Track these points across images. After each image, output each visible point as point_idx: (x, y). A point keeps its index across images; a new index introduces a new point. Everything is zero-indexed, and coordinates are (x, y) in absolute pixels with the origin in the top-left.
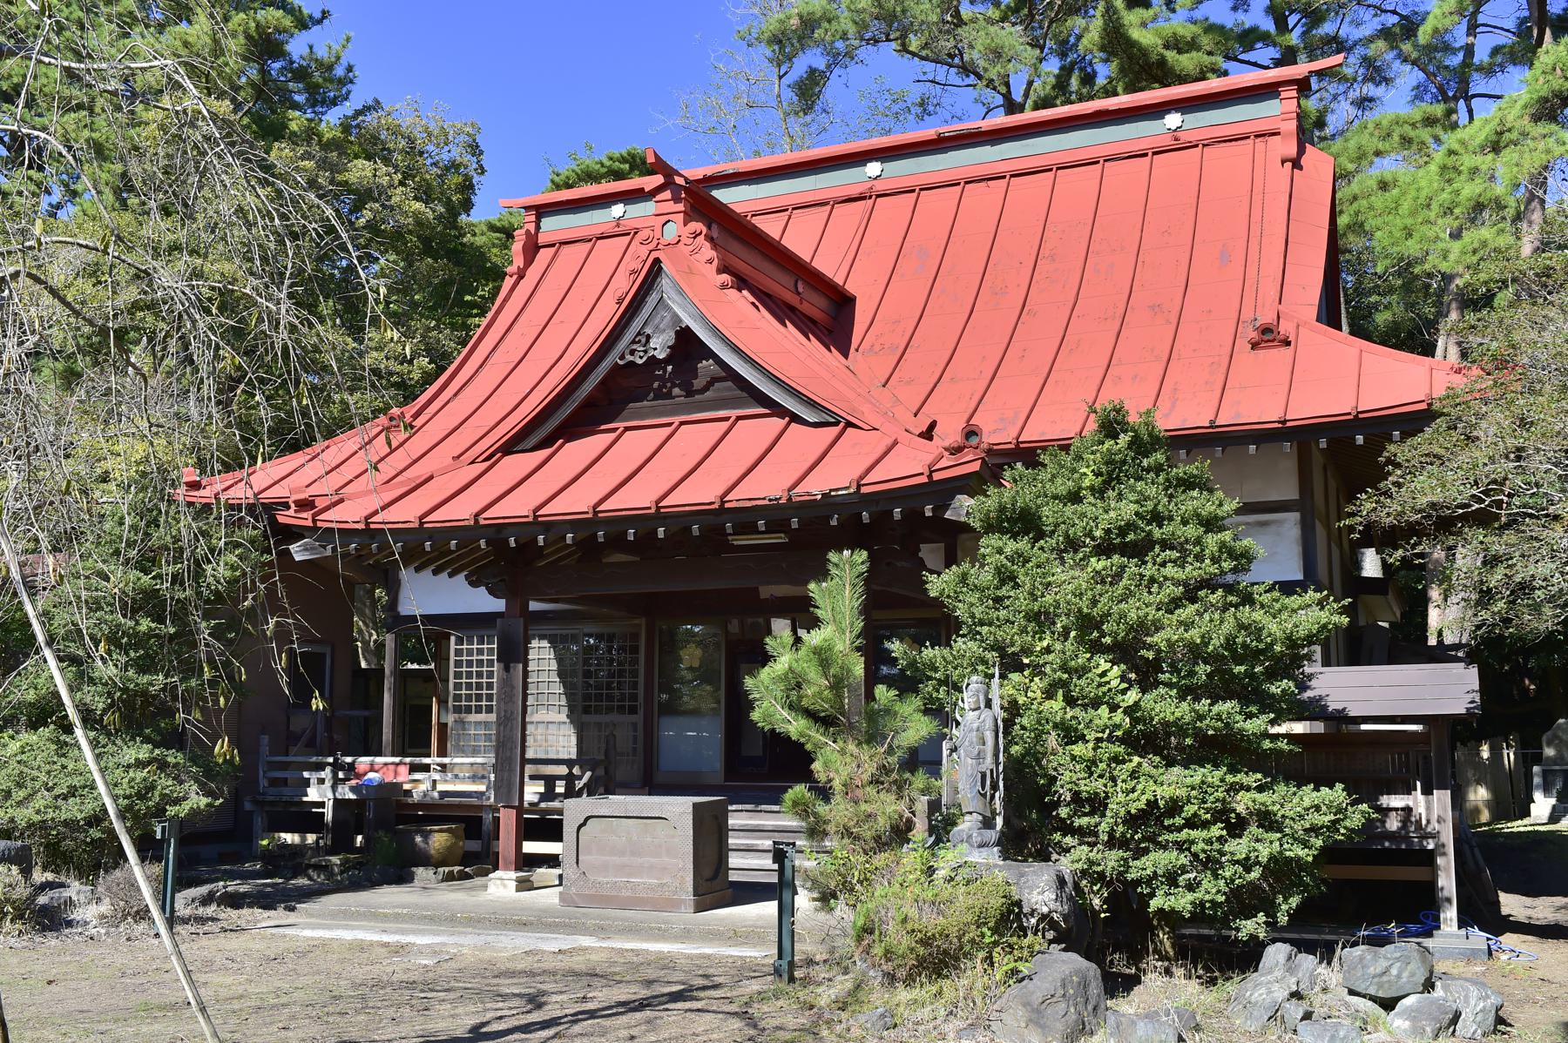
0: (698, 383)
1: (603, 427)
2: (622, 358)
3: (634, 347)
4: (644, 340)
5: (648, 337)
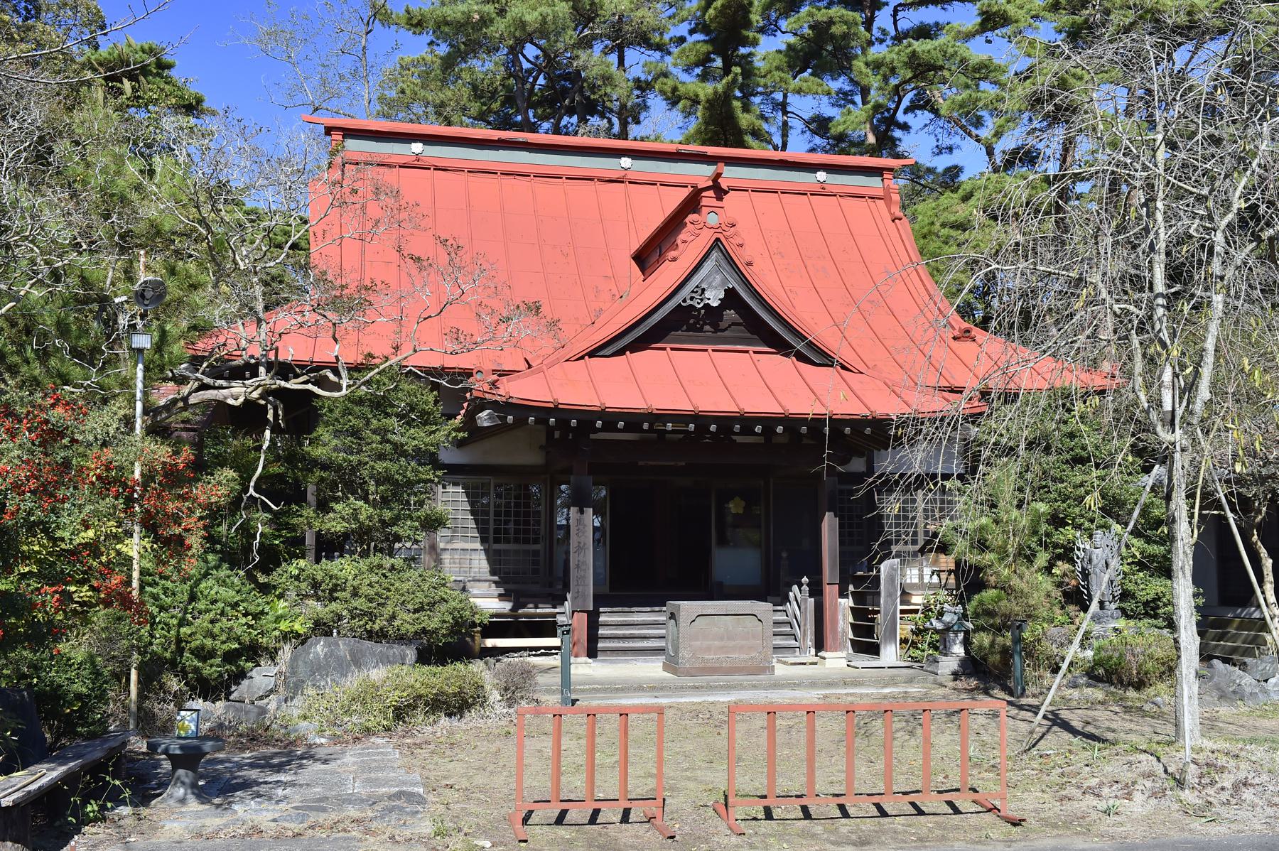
0: (723, 325)
1: (653, 346)
2: (684, 301)
3: (693, 295)
4: (700, 292)
5: (703, 290)
